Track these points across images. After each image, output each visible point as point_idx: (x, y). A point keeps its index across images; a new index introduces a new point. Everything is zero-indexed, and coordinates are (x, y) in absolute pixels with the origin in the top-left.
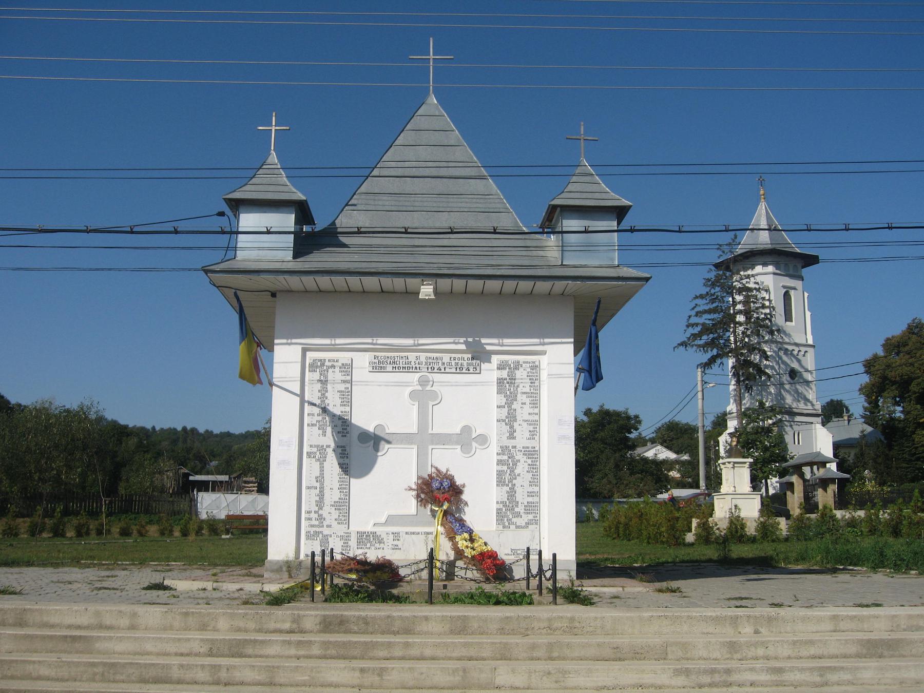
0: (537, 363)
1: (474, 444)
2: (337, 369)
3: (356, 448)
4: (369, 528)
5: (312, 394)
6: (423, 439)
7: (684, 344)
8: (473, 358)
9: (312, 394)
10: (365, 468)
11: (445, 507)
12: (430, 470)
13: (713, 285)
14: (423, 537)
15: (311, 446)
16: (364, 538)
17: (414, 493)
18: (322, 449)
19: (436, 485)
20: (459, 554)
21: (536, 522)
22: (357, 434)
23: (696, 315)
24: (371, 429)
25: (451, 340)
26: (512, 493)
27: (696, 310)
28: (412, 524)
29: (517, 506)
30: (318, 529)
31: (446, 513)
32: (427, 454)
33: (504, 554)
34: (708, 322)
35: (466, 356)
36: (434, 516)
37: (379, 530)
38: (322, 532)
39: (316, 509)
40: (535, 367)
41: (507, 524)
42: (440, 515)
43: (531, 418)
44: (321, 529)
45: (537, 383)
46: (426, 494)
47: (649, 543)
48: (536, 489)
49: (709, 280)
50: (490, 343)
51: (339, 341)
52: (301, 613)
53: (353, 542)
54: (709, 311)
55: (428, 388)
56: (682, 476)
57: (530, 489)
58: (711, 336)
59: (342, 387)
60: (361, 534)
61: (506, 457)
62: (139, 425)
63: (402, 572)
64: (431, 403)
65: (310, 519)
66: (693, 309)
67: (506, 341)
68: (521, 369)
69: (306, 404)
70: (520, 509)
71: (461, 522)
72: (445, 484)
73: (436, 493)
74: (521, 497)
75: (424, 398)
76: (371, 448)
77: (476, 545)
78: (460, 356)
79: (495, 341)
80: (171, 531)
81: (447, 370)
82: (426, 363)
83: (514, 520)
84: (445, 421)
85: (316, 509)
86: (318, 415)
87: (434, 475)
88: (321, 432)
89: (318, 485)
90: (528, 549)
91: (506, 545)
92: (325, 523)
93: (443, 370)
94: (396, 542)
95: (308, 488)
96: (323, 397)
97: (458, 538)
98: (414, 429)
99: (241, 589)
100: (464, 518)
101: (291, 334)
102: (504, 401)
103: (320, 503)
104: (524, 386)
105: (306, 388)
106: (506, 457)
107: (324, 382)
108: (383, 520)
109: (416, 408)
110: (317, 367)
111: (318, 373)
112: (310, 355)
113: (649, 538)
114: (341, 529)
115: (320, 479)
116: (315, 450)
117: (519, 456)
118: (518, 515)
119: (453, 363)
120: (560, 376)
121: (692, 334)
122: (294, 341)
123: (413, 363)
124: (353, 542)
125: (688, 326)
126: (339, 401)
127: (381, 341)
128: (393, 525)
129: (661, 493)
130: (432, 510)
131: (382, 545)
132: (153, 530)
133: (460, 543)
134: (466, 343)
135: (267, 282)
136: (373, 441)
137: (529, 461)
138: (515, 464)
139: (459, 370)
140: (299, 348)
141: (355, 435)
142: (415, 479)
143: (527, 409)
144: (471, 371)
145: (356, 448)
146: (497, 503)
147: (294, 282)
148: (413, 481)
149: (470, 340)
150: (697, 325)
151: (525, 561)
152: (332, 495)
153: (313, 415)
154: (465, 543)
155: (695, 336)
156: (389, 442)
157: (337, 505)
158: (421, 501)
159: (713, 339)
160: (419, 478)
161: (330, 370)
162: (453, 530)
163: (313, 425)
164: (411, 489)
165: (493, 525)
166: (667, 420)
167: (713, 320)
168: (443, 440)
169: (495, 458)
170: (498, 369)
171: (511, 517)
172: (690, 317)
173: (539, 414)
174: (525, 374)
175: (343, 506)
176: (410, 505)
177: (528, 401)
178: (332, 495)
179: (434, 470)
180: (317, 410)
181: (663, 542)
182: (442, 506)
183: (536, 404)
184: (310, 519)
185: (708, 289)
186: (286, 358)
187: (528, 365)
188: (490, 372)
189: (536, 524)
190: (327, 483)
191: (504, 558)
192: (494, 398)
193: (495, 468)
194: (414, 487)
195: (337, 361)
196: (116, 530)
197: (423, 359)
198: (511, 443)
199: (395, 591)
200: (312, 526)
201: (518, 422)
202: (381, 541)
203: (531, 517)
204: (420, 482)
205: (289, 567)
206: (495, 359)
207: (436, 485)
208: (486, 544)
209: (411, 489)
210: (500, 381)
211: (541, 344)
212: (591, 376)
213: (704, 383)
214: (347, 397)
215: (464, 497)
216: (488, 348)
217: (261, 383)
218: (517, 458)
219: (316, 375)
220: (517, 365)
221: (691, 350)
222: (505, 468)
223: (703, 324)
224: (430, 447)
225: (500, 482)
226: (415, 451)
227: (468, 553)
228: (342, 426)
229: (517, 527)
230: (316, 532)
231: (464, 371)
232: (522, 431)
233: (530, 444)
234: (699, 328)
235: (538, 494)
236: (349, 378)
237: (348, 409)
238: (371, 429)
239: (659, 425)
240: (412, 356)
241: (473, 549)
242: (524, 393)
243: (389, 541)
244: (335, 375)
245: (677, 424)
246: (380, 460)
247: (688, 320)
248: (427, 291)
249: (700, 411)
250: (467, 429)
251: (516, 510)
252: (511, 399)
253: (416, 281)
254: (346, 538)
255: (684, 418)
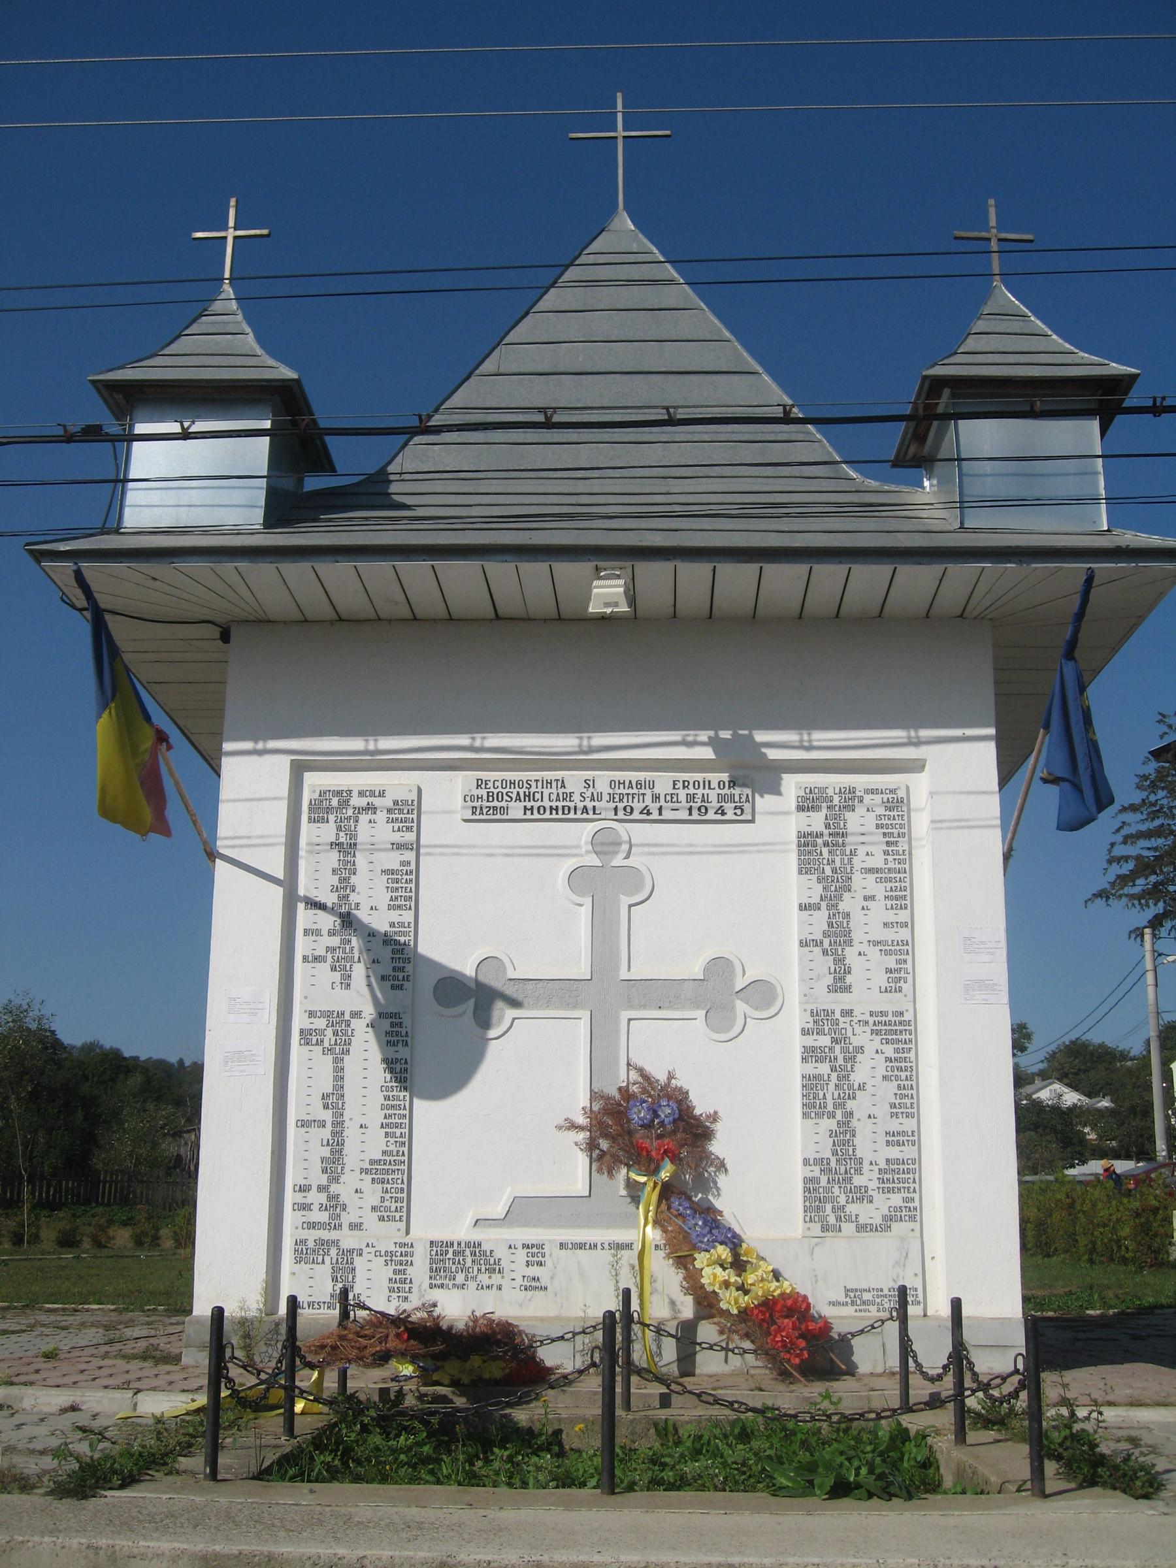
0: (901, 793)
1: (741, 1007)
2: (381, 816)
3: (430, 1020)
4: (462, 1232)
5: (317, 878)
6: (606, 993)
7: (1102, 894)
8: (733, 783)
9: (317, 878)
10: (453, 1076)
11: (664, 1175)
12: (622, 1076)
13: (1153, 787)
14: (606, 1256)
15: (312, 1014)
16: (451, 1260)
17: (582, 1136)
18: (339, 1021)
19: (639, 1114)
20: (706, 1303)
21: (911, 1213)
22: (432, 981)
23: (1125, 842)
24: (468, 969)
25: (676, 736)
26: (844, 1136)
27: (1124, 832)
28: (575, 1221)
29: (859, 1171)
30: (325, 1235)
31: (667, 1191)
32: (617, 1031)
33: (827, 1303)
34: (1146, 853)
35: (715, 777)
36: (635, 1200)
37: (490, 1237)
38: (336, 1243)
39: (324, 1179)
40: (897, 804)
41: (832, 1220)
42: (651, 1196)
43: (889, 935)
44: (333, 1235)
45: (903, 845)
46: (612, 1138)
47: (1091, 1261)
48: (909, 1125)
49: (1145, 777)
50: (777, 743)
51: (387, 743)
52: (122, 1543)
53: (419, 1271)
54: (1148, 835)
55: (618, 861)
56: (1100, 1138)
57: (894, 1125)
58: (1153, 878)
59: (393, 860)
60: (440, 1248)
61: (825, 1041)
62: (156, 1056)
63: (549, 1356)
64: (625, 901)
65: (305, 1207)
66: (1118, 831)
67: (820, 737)
68: (860, 810)
69: (301, 906)
70: (867, 1179)
71: (710, 1215)
72: (666, 1111)
73: (640, 1137)
74: (869, 1145)
75: (607, 887)
76: (468, 1019)
77: (751, 1278)
78: (699, 776)
79: (791, 736)
80: (156, 1238)
81: (667, 814)
82: (612, 798)
83: (852, 1209)
84: (663, 946)
85: (324, 1179)
86: (332, 933)
87: (635, 1089)
88: (337, 976)
89: (327, 1116)
90: (903, 1291)
91: (832, 1277)
92: (346, 1219)
93: (655, 815)
94: (534, 1271)
95: (303, 1124)
96: (344, 886)
97: (701, 1259)
98: (582, 970)
99: (74, 1408)
100: (718, 1204)
101: (266, 728)
102: (816, 892)
103: (333, 1165)
104: (870, 852)
105: (302, 864)
106: (825, 1041)
107: (346, 848)
108: (499, 1210)
109: (585, 912)
110: (329, 810)
111: (332, 826)
112: (314, 781)
113: (1093, 1251)
114: (387, 1235)
115: (334, 1100)
116: (320, 1023)
117: (861, 1037)
118: (862, 1195)
119: (682, 794)
120: (963, 824)
121: (1118, 876)
122: (272, 744)
123: (576, 797)
124: (419, 1271)
125: (1110, 862)
126: (383, 899)
127: (495, 740)
128: (526, 1224)
129: (1072, 1166)
130: (631, 1185)
131: (496, 1279)
132: (122, 1237)
133: (707, 1272)
134: (713, 742)
135: (196, 585)
136: (474, 1002)
137: (889, 1050)
138: (851, 1059)
139: (699, 813)
140: (286, 760)
141: (426, 984)
142: (583, 1100)
143: (879, 911)
144: (730, 815)
145: (430, 1020)
146: (806, 1162)
147: (268, 587)
148: (577, 1102)
149: (726, 735)
150: (1126, 859)
151: (893, 1327)
152: (366, 1143)
153: (318, 933)
154: (722, 1275)
155: (1123, 880)
156: (515, 1003)
157: (378, 1170)
158: (600, 1158)
159: (1156, 885)
160: (594, 1096)
161: (364, 818)
162: (686, 1236)
163: (317, 959)
164: (573, 1126)
165: (794, 1223)
166: (1073, 1036)
167: (1156, 849)
168: (661, 995)
169: (797, 1043)
170: (800, 809)
171: (842, 1200)
172: (1113, 845)
173: (909, 925)
174: (870, 821)
175: (394, 1173)
176: (573, 1170)
177: (880, 890)
178: (366, 1143)
179: (634, 1075)
180: (327, 921)
181: (1125, 1261)
182: (656, 1171)
183: (901, 898)
184: (305, 1207)
185: (1144, 794)
186: (251, 788)
187: (878, 798)
188: (780, 816)
189: (912, 1219)
190: (351, 1111)
191: (828, 1312)
192: (791, 885)
193: (797, 1069)
194: (581, 1120)
195: (382, 794)
196: (49, 1234)
197: (602, 786)
198: (839, 1002)
199: (521, 1416)
200: (313, 1226)
201: (857, 948)
202: (494, 1268)
203: (896, 1200)
204: (596, 1108)
205: (247, 1336)
206: (792, 784)
207: (639, 1114)
208: (777, 1275)
209: (573, 1126)
210: (806, 841)
211: (910, 743)
212: (1078, 788)
213: (1158, 955)
214: (405, 886)
215: (717, 1147)
216: (773, 754)
217: (165, 831)
218: (856, 1041)
219: (328, 832)
220: (850, 800)
221: (1118, 905)
222: (824, 1069)
223: (1138, 858)
224: (625, 1015)
225: (813, 1107)
226: (583, 1027)
227: (730, 1301)
228: (394, 961)
229: (861, 1228)
230: (321, 1242)
231: (711, 815)
232: (867, 969)
233: (889, 1003)
234: (1131, 865)
235: (913, 1139)
236: (411, 837)
237: (408, 917)
238: (469, 970)
239: (1053, 1047)
240: (574, 780)
241: (743, 1289)
242: (871, 871)
243: (517, 1266)
244: (375, 831)
245: (1085, 1045)
246: (494, 1049)
247: (1110, 851)
248: (607, 593)
249: (1152, 1008)
250: (720, 967)
251: (858, 1181)
252: (836, 886)
253: (583, 568)
254: (400, 1258)
255: (1102, 1035)
